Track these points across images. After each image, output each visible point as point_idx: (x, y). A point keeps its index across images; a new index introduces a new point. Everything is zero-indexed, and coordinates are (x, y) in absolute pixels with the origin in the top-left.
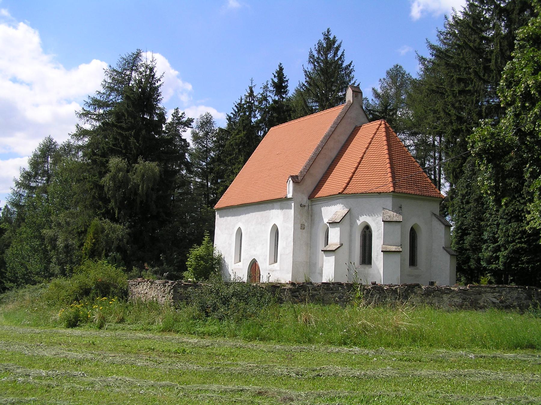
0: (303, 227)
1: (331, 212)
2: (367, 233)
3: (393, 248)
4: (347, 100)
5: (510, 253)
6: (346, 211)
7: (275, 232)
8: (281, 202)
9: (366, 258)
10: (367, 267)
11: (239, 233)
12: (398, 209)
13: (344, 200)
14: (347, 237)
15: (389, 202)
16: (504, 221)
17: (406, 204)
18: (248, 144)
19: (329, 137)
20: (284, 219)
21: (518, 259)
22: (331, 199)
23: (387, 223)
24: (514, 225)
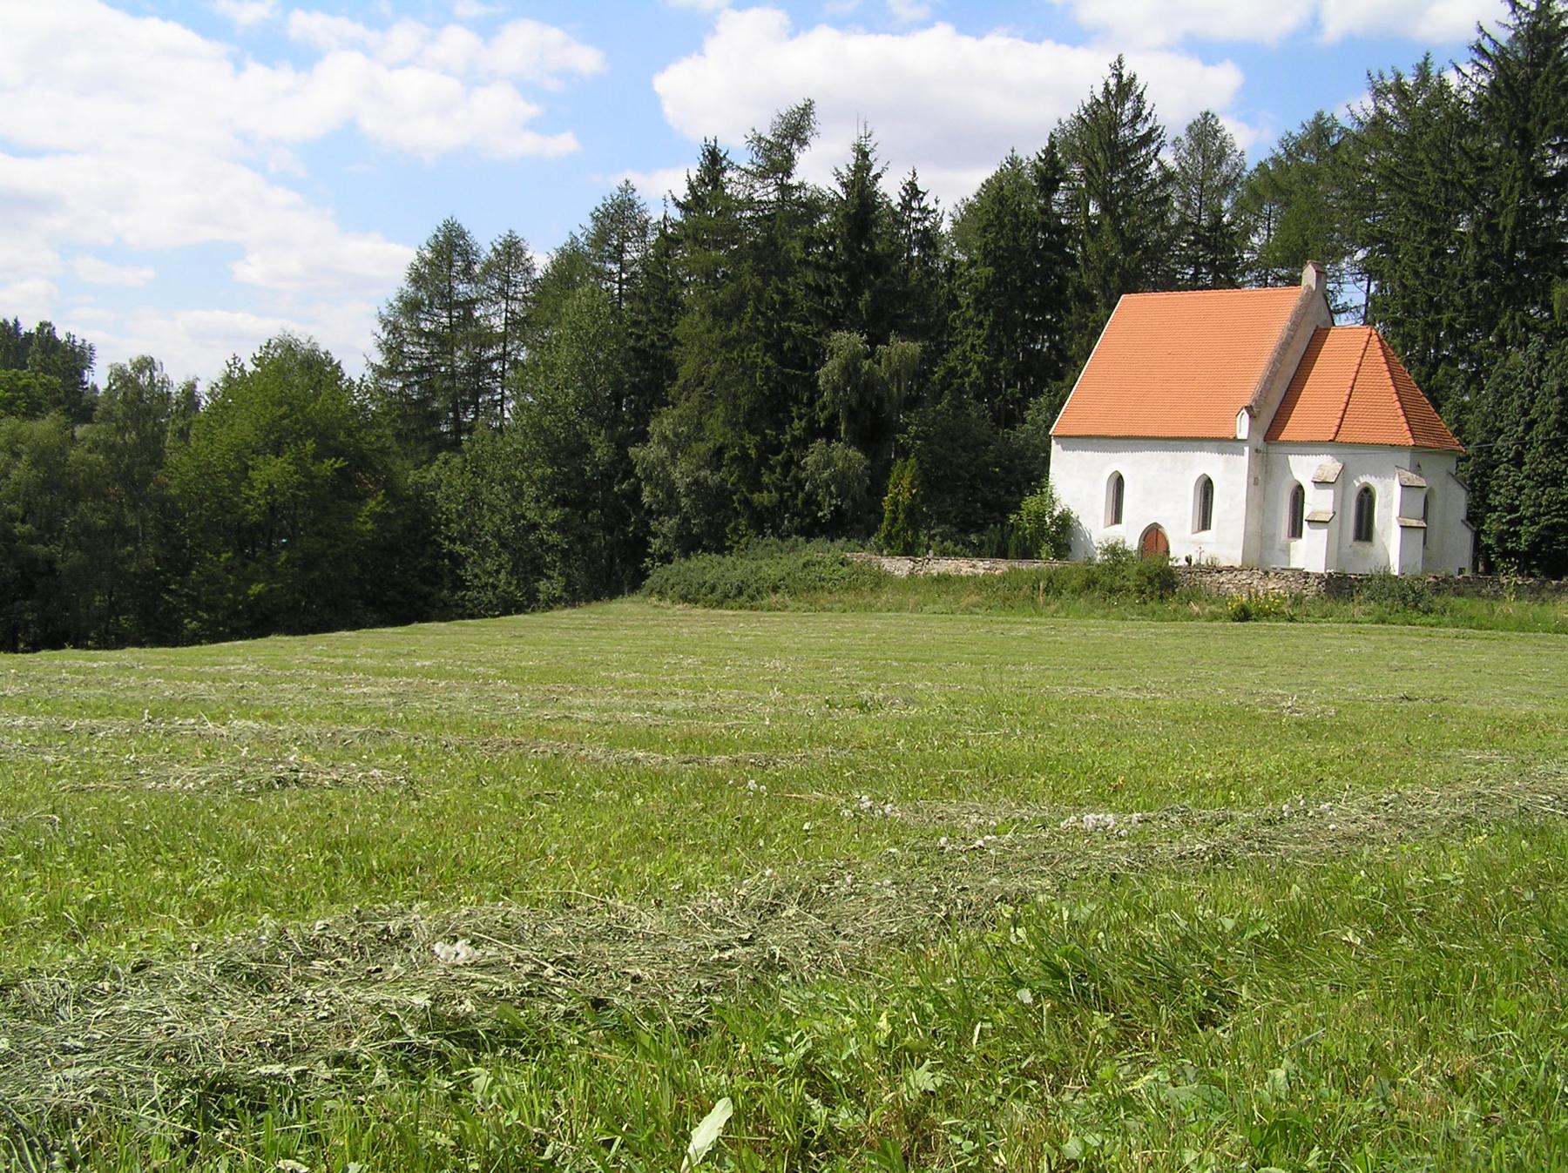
0: (1256, 484)
1: (1305, 468)
2: (1366, 499)
3: (1414, 523)
4: (1304, 283)
5: (1543, 529)
6: (1338, 466)
7: (1206, 488)
8: (1226, 443)
9: (1365, 530)
10: (1367, 545)
11: (1118, 482)
12: (1417, 469)
13: (1334, 451)
14: (1340, 502)
15: (1405, 459)
16: (1532, 483)
17: (1427, 462)
18: (926, 263)
19: (1285, 346)
20: (1232, 475)
21: (1552, 539)
22: (1309, 446)
23: (1411, 492)
24: (1551, 490)
